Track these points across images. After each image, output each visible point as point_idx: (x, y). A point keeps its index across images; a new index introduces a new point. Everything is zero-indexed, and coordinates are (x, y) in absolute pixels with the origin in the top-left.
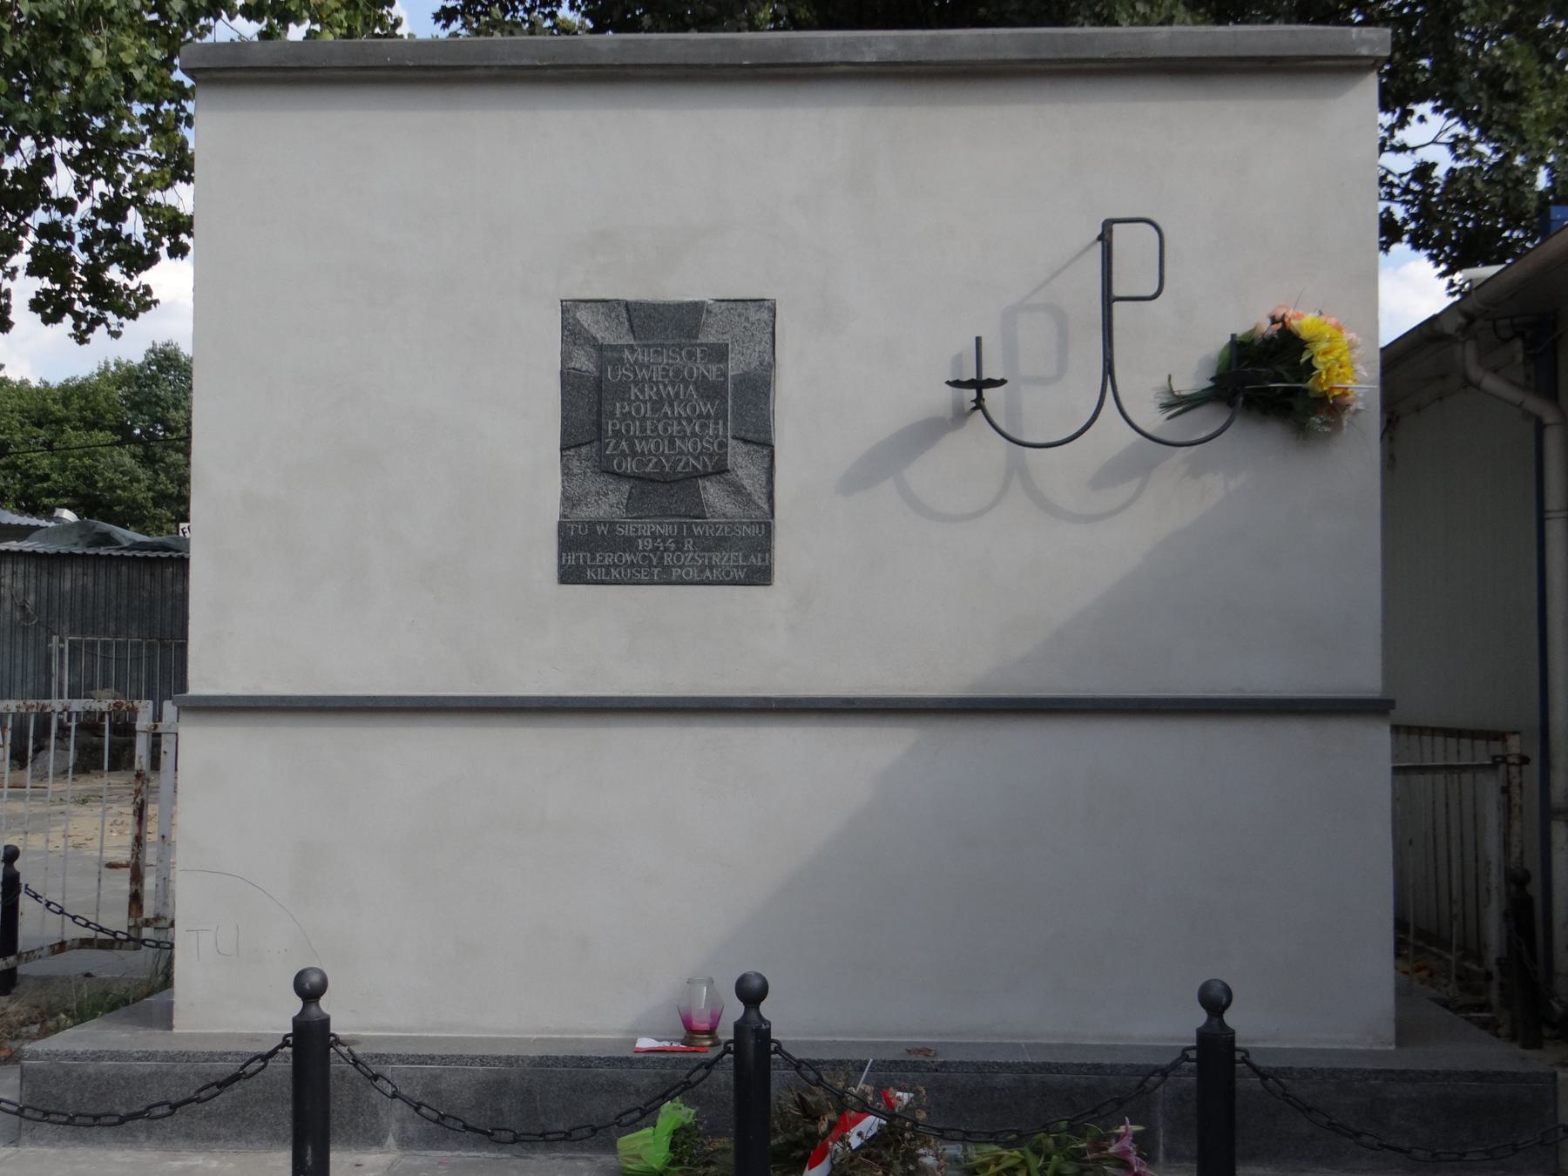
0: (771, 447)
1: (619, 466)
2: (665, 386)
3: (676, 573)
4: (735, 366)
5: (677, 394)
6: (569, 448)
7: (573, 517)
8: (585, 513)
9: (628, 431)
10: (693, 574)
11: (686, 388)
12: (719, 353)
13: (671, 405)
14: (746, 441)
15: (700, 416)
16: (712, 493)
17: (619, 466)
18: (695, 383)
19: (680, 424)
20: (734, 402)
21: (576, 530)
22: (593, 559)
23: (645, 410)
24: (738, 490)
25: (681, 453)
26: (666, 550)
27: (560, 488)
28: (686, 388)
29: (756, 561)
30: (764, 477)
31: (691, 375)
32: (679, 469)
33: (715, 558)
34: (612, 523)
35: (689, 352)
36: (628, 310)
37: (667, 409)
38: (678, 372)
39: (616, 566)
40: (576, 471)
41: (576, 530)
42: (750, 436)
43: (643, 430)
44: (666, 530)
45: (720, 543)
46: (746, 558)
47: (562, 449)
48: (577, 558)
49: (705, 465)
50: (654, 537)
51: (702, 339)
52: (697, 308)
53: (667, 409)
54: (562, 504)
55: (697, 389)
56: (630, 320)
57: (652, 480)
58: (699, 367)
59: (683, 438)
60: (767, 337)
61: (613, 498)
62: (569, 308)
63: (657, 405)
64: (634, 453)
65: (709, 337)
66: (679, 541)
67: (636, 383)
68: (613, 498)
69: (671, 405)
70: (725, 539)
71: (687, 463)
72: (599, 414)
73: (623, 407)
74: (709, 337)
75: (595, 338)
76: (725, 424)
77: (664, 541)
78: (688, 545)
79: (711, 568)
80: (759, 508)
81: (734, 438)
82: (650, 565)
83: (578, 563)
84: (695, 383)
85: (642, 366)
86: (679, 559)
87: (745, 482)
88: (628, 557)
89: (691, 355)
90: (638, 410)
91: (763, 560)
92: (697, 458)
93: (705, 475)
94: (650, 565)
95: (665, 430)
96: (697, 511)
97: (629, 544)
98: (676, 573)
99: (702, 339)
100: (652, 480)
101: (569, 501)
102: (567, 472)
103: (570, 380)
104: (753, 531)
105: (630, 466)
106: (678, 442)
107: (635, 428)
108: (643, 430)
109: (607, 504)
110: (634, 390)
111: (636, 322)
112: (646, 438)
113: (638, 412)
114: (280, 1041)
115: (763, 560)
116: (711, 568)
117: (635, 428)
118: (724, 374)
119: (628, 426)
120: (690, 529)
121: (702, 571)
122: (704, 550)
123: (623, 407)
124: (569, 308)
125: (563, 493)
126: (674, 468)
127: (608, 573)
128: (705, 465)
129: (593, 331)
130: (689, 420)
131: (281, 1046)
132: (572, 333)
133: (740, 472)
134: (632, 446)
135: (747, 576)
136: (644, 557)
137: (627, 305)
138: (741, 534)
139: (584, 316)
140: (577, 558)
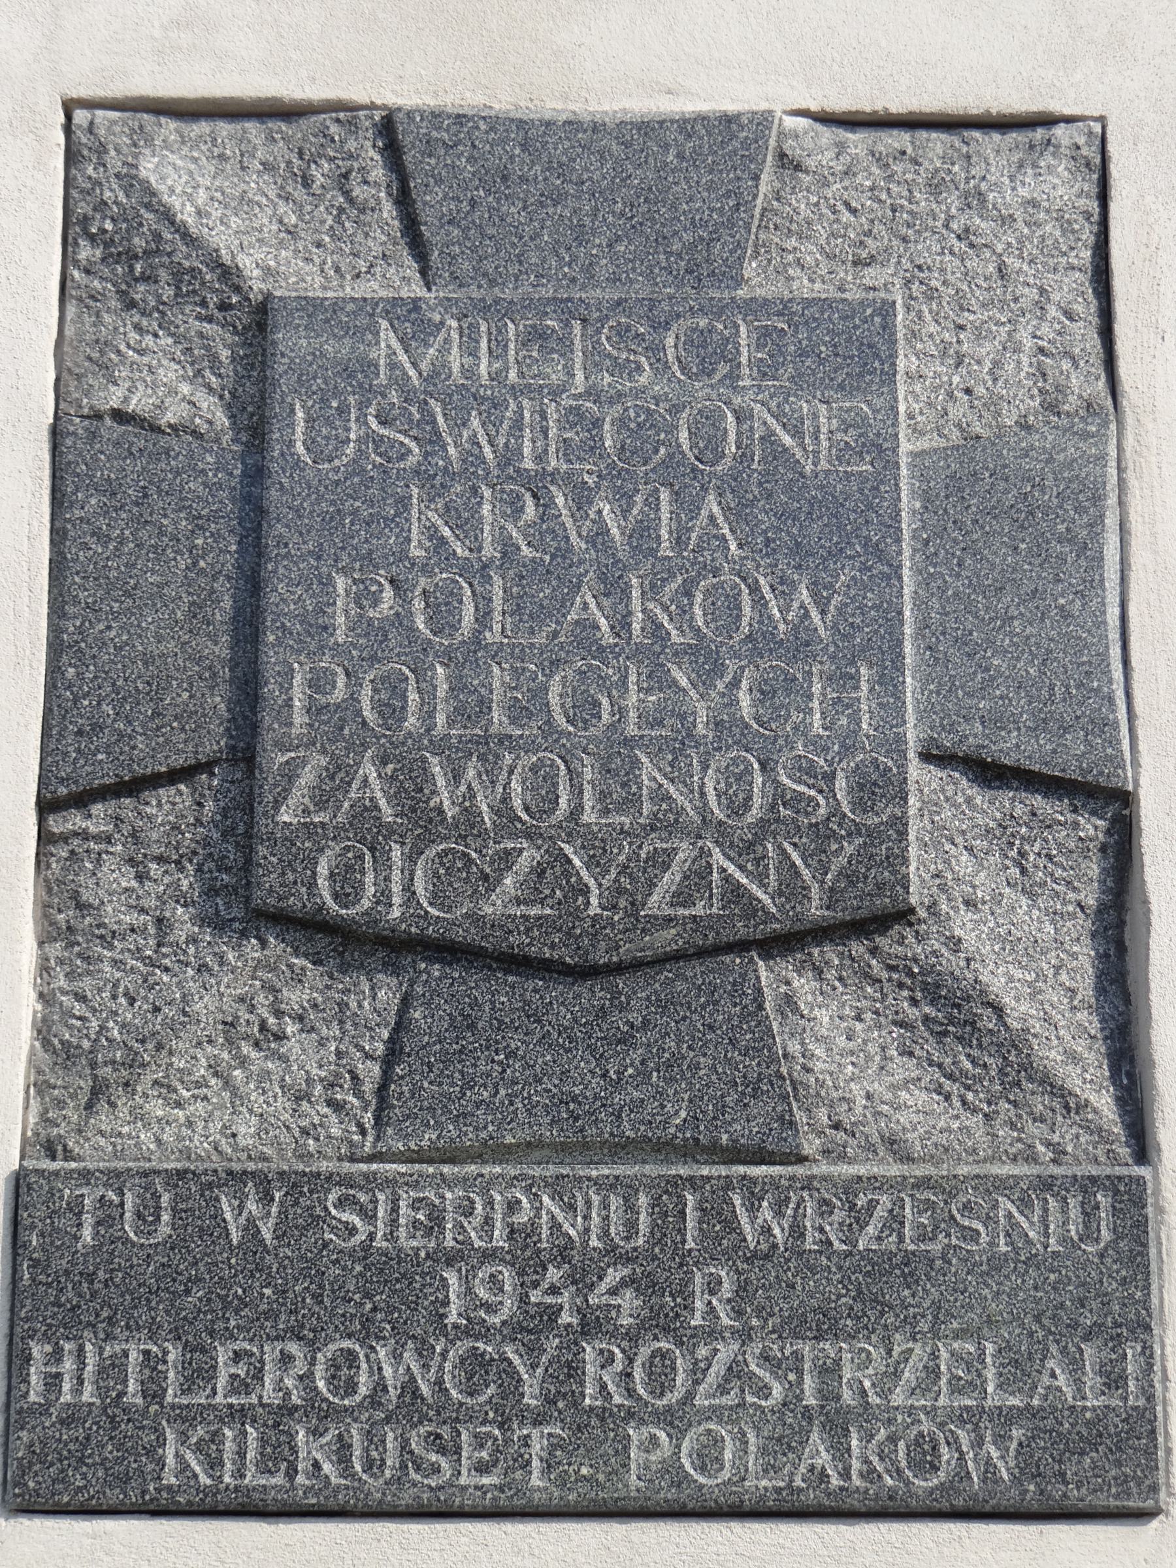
0: (1117, 807)
1: (346, 883)
2: (581, 499)
3: (647, 1451)
4: (921, 407)
5: (643, 532)
6: (82, 800)
7: (92, 1152)
8: (158, 1128)
9: (391, 712)
10: (742, 1462)
11: (687, 505)
12: (855, 347)
13: (612, 587)
14: (990, 773)
15: (761, 642)
16: (833, 1032)
17: (346, 883)
18: (733, 483)
19: (657, 678)
20: (925, 580)
21: (108, 1217)
22: (198, 1374)
23: (485, 611)
24: (953, 1015)
25: (668, 823)
26: (592, 1324)
27: (27, 1006)
28: (687, 505)
29: (1070, 1383)
30: (1084, 957)
31: (710, 450)
32: (656, 903)
33: (859, 1369)
34: (302, 1185)
35: (697, 341)
36: (393, 151)
37: (587, 603)
38: (644, 431)
39: (321, 1414)
40: (117, 915)
41: (108, 1217)
42: (1010, 747)
43: (472, 708)
44: (592, 1221)
45: (880, 1291)
46: (1019, 1368)
47: (46, 806)
48: (113, 1369)
49: (791, 888)
50: (527, 1253)
51: (756, 279)
52: (731, 140)
53: (587, 603)
54: (39, 1086)
55: (738, 514)
56: (404, 199)
57: (518, 963)
58: (750, 409)
59: (678, 747)
60: (1072, 288)
61: (305, 1056)
62: (96, 137)
63: (541, 581)
64: (422, 822)
65: (795, 269)
66: (661, 1280)
67: (433, 482)
68: (305, 1056)
69: (612, 587)
70: (909, 1268)
71: (699, 875)
72: (248, 627)
73: (365, 596)
74: (795, 269)
75: (228, 273)
76: (889, 681)
77: (582, 1280)
78: (711, 1297)
79: (837, 1426)
80: (1070, 1105)
81: (932, 756)
82: (508, 1411)
83: (112, 1407)
84: (733, 483)
85: (466, 398)
86: (660, 1380)
87: (999, 978)
88: (388, 1365)
89: (709, 354)
90: (442, 612)
91: (1114, 1380)
92: (747, 850)
93: (777, 945)
94: (508, 1411)
95: (584, 710)
96: (753, 1124)
97: (394, 1293)
98: (647, 1451)
99: (756, 279)
100: (518, 963)
101: (76, 1064)
102: (66, 921)
103: (89, 454)
104: (1055, 1226)
105: (400, 889)
106: (648, 772)
107: (430, 706)
108: (472, 708)
109: (260, 1081)
110: (423, 518)
111: (432, 203)
112: (488, 749)
113: (442, 612)
114: (1096, 114)
115: (1114, 1380)
116: (837, 1426)
117: (430, 706)
118: (882, 451)
119: (394, 686)
120: (717, 1215)
121: (783, 1445)
122: (794, 1326)
123: (365, 596)
124: (96, 137)
125: (43, 1031)
126: (627, 898)
127: (279, 1453)
128: (791, 888)
129: (221, 239)
130: (706, 661)
131: (1095, 119)
132: (118, 248)
133: (963, 924)
134: (411, 789)
135: (1028, 1468)
136: (476, 1368)
137: (388, 128)
138: (990, 1240)
139: (179, 173)
140: (113, 1369)
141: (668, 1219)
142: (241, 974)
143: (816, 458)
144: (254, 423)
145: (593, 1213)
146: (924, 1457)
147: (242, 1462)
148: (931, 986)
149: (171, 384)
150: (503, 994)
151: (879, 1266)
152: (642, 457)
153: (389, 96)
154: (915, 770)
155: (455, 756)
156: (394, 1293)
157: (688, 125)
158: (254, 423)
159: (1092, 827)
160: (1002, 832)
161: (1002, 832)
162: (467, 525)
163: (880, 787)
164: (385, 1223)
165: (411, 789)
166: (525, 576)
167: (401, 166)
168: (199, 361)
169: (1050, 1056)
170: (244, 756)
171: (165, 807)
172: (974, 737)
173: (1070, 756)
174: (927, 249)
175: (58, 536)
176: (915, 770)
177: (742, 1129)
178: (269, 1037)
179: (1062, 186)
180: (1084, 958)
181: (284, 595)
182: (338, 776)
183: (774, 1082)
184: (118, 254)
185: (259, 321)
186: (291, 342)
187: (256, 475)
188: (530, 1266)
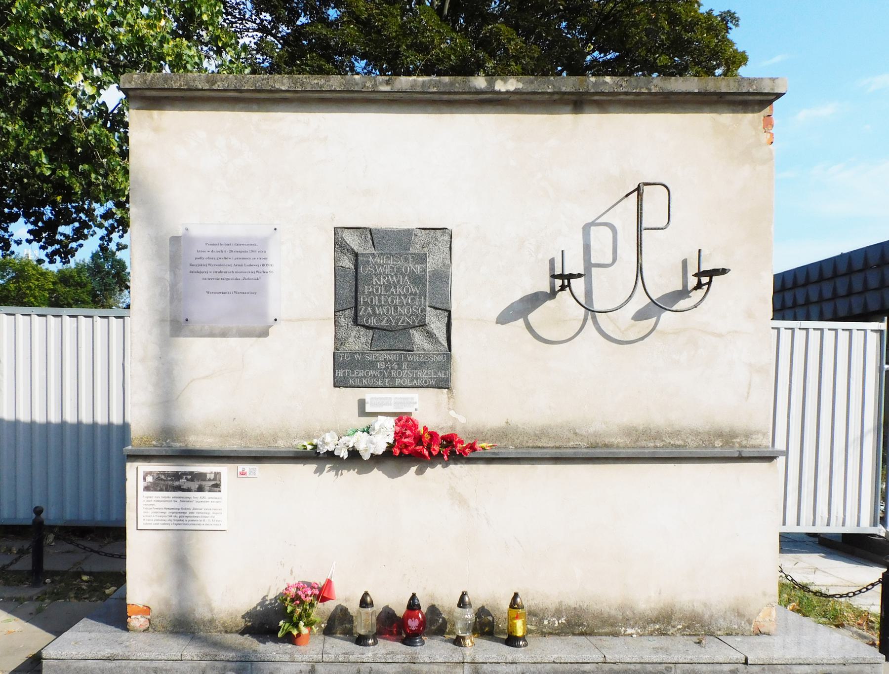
0: (450, 312)
1: (367, 320)
3: (398, 382)
4: (431, 264)
5: (399, 281)
9: (372, 302)
11: (404, 278)
12: (422, 259)
13: (395, 288)
15: (411, 294)
16: (417, 336)
17: (367, 320)
18: (409, 275)
19: (400, 298)
24: (430, 335)
25: (401, 314)
28: (404, 278)
29: (441, 375)
33: (419, 373)
37: (393, 290)
38: (399, 269)
43: (380, 301)
45: (422, 365)
46: (436, 373)
49: (414, 322)
50: (386, 361)
51: (412, 250)
52: (409, 233)
53: (393, 290)
63: (388, 287)
67: (376, 275)
68: (363, 340)
69: (395, 288)
70: (425, 363)
71: (404, 321)
76: (425, 298)
77: (392, 364)
78: (405, 366)
79: (417, 380)
80: (443, 345)
84: (409, 275)
85: (379, 265)
87: (436, 331)
88: (372, 372)
89: (406, 260)
90: (377, 290)
92: (409, 318)
97: (372, 365)
98: (398, 382)
99: (412, 250)
103: (338, 271)
105: (373, 322)
108: (380, 301)
110: (375, 279)
112: (382, 306)
118: (425, 271)
121: (412, 381)
122: (413, 369)
126: (397, 323)
127: (361, 381)
128: (414, 322)
129: (352, 245)
132: (340, 246)
133: (432, 325)
134: (374, 311)
141: (400, 358)
142: (354, 331)
143: (418, 272)
144: (356, 268)
145: (393, 356)
146: (426, 382)
147: (357, 382)
148: (428, 332)
149: (347, 263)
150: (383, 333)
151: (422, 362)
152: (399, 272)
153: (371, 227)
154: (428, 308)
155: (378, 306)
156: (372, 365)
157: (404, 231)
158: (356, 268)
159: (446, 314)
160: (437, 315)
161: (437, 315)
162: (380, 280)
163: (423, 310)
164: (371, 358)
165: (374, 311)
166: (386, 286)
167: (371, 235)
168: (350, 260)
169: (440, 340)
170: (356, 307)
171: (347, 312)
172: (434, 304)
173: (444, 306)
174: (431, 245)
175: (427, 387)
176: (428, 308)
177: (409, 348)
178: (359, 338)
179: (447, 238)
180: (445, 328)
181: (360, 288)
182: (366, 309)
183: (411, 342)
184: (340, 246)
185: (356, 255)
186: (360, 258)
187: (357, 274)
188: (386, 363)
